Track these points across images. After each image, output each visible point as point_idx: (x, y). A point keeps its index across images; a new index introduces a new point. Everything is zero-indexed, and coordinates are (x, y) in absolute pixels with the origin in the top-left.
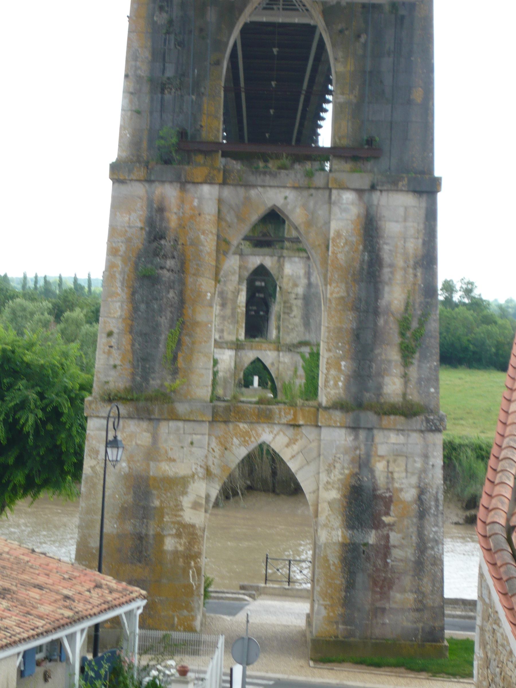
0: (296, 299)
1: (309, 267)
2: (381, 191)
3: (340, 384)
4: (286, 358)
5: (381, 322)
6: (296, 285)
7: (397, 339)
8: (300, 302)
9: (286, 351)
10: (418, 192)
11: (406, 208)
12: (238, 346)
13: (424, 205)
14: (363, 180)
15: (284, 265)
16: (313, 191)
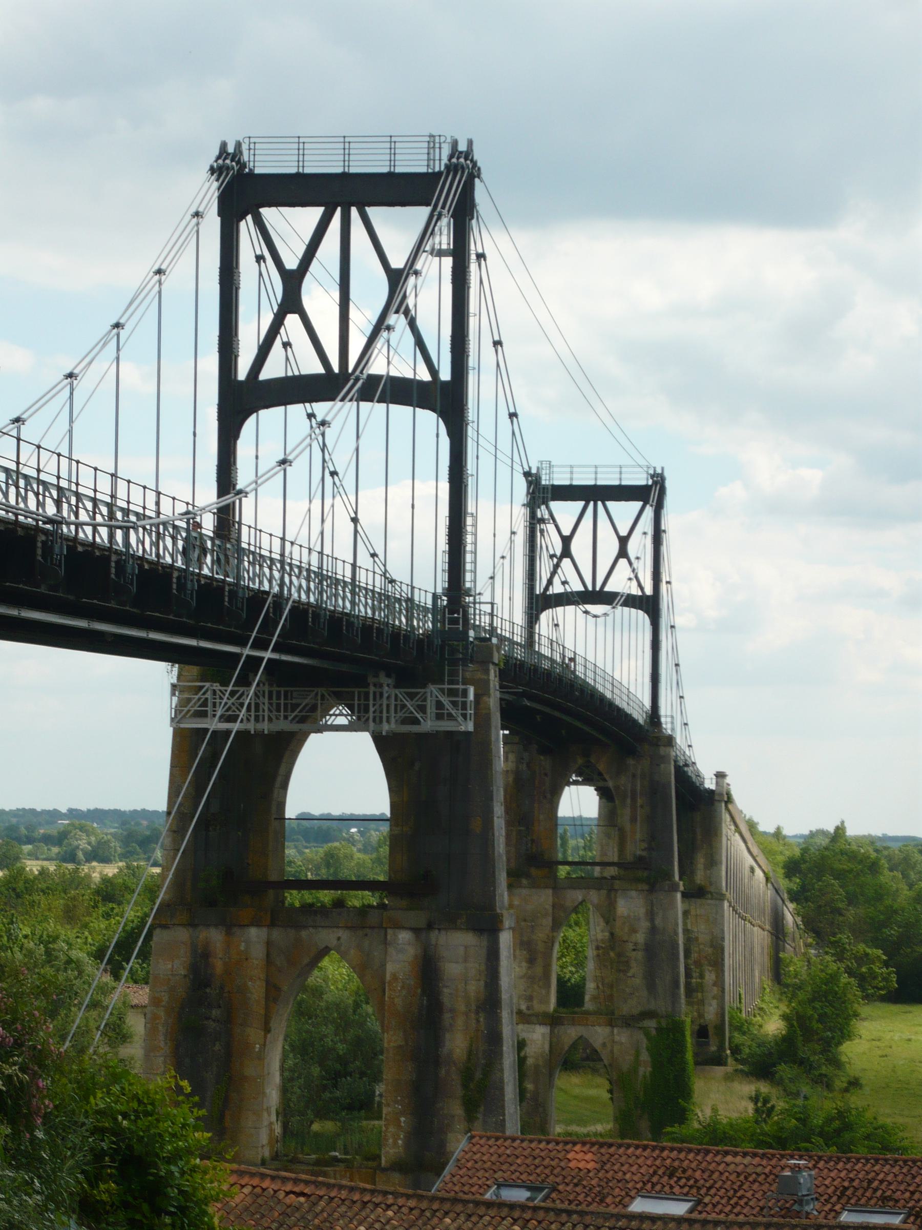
0: (634, 950)
1: (652, 905)
2: (439, 930)
3: (400, 1142)
4: (623, 1037)
5: (443, 1072)
6: (634, 931)
7: (459, 1092)
8: (640, 955)
9: (622, 1027)
11: (466, 947)
12: (553, 1021)
13: (485, 943)
14: (419, 918)
15: (616, 901)
16: (368, 930)
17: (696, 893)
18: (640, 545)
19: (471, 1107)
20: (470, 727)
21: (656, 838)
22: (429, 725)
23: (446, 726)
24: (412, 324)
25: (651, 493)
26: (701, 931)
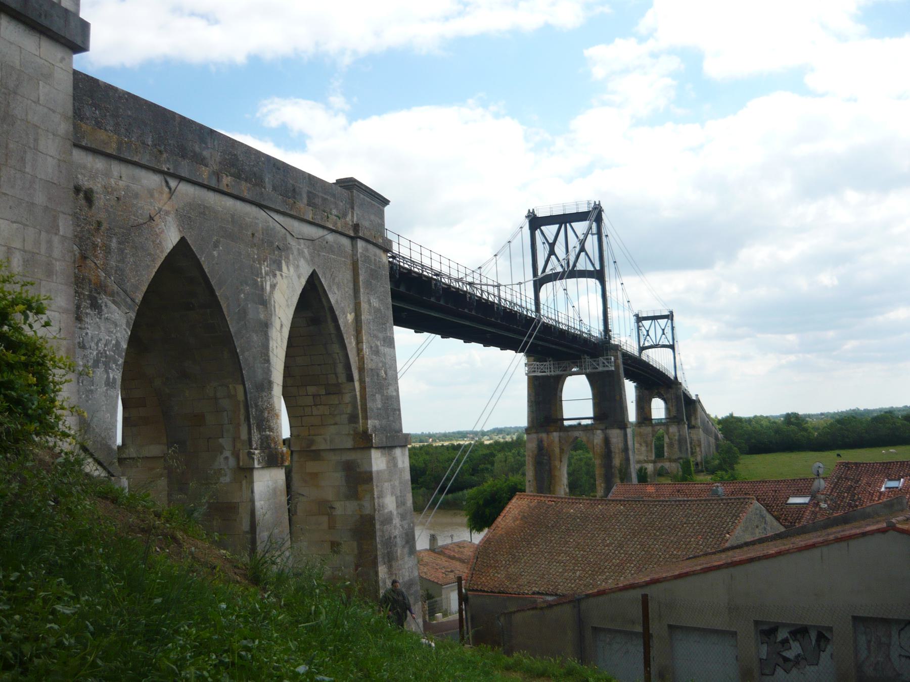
4: (673, 465)
7: (618, 475)
10: (620, 428)
12: (654, 462)
17: (691, 427)
18: (668, 331)
19: (622, 480)
20: (613, 369)
21: (679, 410)
22: (601, 369)
23: (606, 369)
24: (577, 237)
25: (670, 317)
26: (694, 437)
